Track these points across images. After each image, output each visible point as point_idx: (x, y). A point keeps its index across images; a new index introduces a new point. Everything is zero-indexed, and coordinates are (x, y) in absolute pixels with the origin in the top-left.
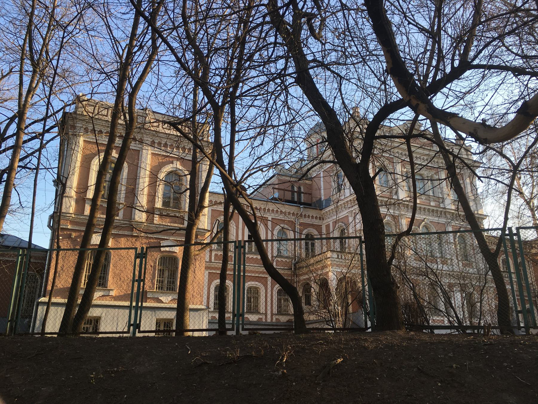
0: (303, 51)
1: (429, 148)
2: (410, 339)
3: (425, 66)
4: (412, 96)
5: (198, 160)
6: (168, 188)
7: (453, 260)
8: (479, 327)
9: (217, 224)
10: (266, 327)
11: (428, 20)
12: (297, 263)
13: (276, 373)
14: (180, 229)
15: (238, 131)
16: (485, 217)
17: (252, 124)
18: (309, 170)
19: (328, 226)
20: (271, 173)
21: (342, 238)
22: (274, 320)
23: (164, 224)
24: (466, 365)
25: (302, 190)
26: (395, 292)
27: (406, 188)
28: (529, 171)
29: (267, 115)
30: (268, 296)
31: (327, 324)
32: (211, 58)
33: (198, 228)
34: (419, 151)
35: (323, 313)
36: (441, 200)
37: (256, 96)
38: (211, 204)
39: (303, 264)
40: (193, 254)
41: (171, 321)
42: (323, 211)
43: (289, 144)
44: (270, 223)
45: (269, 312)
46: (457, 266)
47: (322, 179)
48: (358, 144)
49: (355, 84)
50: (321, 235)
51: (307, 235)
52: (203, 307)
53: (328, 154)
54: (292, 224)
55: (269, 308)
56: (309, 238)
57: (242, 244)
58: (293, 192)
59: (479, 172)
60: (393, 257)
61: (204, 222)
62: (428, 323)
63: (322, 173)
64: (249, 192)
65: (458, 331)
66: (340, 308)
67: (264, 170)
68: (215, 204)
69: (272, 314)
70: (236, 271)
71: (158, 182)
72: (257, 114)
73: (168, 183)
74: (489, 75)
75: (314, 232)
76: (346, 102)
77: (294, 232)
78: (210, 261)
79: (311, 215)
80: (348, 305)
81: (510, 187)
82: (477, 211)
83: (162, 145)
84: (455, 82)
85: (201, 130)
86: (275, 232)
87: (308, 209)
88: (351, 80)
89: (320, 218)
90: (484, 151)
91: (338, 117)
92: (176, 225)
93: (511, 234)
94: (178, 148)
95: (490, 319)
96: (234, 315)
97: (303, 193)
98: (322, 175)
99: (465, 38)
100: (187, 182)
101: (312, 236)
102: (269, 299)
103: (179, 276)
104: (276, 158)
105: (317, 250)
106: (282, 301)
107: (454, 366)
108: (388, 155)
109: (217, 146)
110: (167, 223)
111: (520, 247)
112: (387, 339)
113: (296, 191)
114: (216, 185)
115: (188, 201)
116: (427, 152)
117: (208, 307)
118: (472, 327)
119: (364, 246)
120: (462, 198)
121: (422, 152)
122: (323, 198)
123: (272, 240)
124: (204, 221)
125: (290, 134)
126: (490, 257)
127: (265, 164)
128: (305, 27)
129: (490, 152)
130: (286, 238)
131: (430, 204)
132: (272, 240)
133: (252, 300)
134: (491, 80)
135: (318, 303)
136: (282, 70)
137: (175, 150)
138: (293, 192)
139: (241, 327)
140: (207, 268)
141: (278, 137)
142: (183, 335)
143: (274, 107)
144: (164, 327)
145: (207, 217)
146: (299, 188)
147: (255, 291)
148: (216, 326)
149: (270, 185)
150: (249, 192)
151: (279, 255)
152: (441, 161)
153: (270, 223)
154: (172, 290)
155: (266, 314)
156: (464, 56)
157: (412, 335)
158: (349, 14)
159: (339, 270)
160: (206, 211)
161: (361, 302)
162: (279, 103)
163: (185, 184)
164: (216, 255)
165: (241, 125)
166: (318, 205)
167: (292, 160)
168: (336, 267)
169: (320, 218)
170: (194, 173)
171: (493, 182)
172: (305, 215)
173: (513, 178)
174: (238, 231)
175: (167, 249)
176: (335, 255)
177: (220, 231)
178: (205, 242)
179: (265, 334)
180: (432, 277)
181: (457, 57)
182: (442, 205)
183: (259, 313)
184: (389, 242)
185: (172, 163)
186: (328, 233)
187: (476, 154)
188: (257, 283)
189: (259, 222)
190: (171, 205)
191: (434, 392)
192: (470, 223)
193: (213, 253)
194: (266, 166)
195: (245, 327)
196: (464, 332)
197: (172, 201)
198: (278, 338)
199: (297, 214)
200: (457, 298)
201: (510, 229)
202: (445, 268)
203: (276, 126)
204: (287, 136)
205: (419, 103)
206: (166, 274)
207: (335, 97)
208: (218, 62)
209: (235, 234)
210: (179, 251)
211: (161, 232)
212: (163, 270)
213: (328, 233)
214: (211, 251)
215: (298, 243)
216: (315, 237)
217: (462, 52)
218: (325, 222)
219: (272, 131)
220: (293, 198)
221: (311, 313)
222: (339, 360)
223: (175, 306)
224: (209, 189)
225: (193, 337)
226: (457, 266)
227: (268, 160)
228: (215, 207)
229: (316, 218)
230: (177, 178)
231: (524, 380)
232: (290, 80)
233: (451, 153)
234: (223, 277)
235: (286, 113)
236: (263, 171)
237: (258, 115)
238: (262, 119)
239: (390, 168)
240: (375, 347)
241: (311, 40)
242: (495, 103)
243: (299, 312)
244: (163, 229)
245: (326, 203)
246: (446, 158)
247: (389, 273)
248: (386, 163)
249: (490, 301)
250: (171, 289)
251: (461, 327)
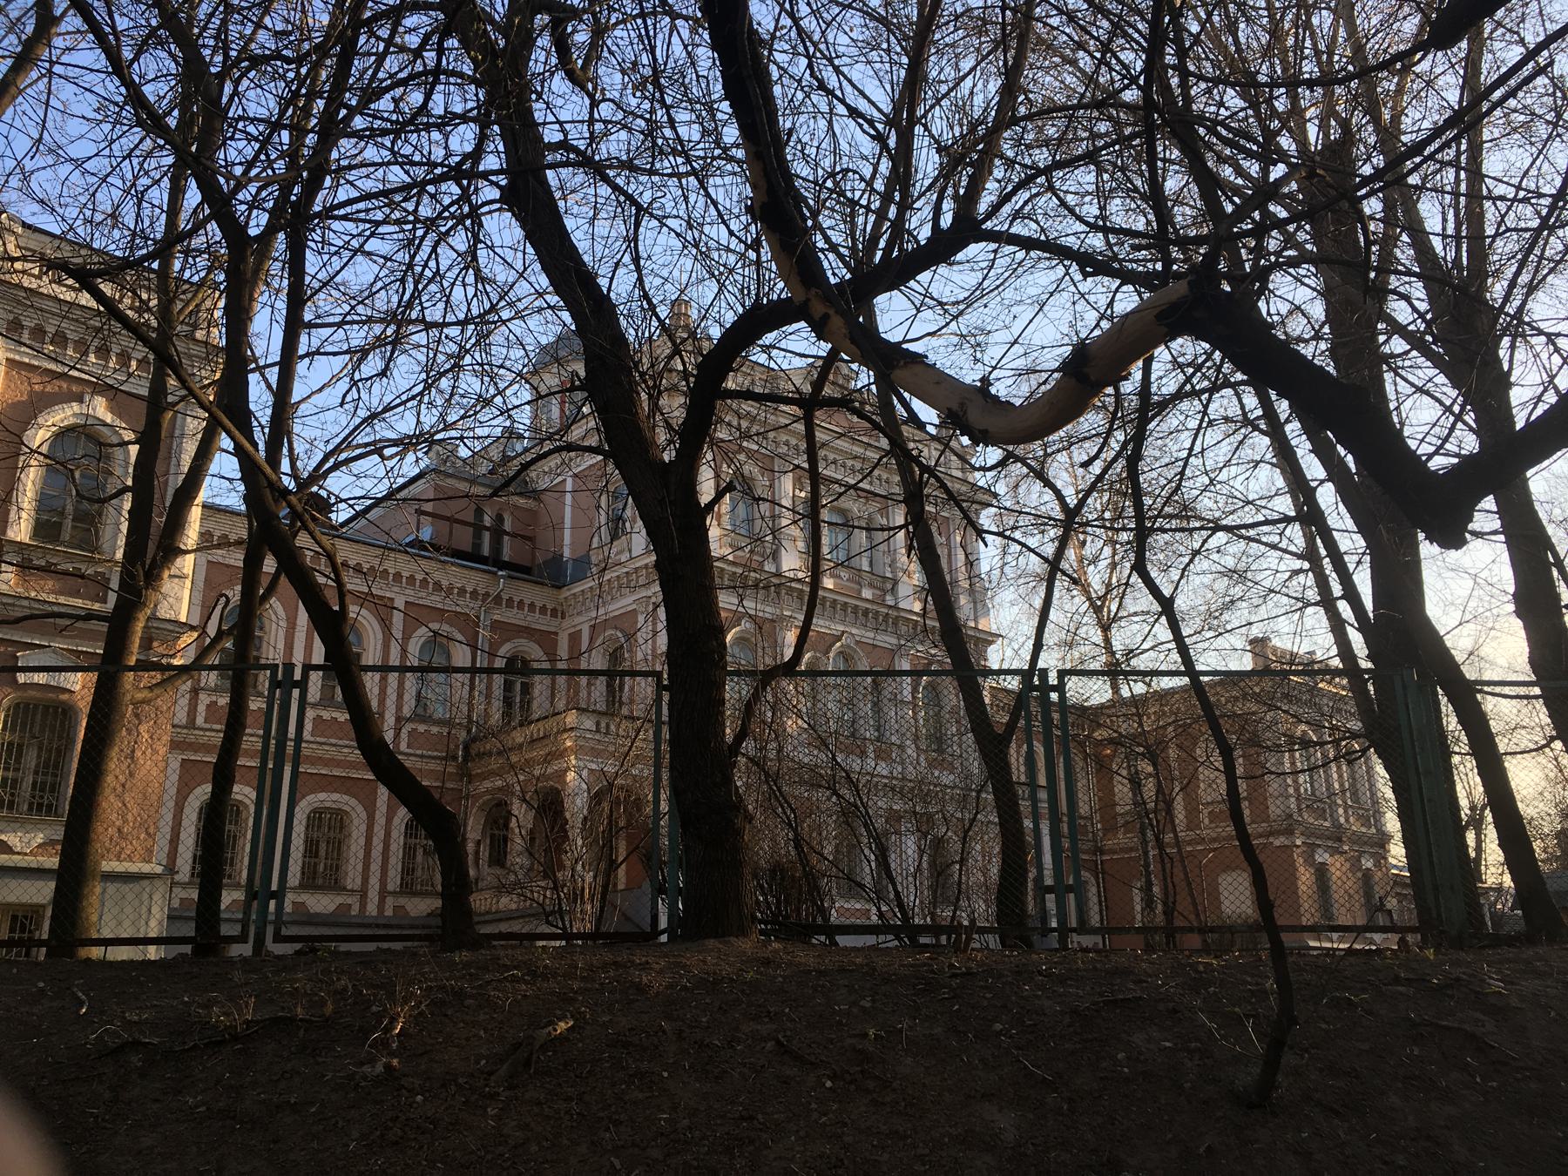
0: (530, 112)
1: (865, 439)
2: (767, 962)
3: (872, 218)
4: (813, 291)
5: (170, 399)
6: (61, 480)
7: (906, 748)
8: (953, 928)
9: (219, 608)
10: (355, 932)
11: (888, 87)
12: (474, 740)
13: (367, 1069)
14: (90, 616)
15: (310, 325)
16: (990, 638)
17: (360, 309)
18: (525, 467)
19: (575, 638)
20: (410, 466)
21: (615, 674)
22: (389, 912)
23: (33, 594)
24: (901, 1031)
25: (507, 526)
26: (739, 833)
27: (801, 545)
28: (1103, 527)
29: (410, 286)
30: (378, 833)
31: (548, 922)
32: (237, 83)
33: (153, 617)
34: (842, 444)
35: (541, 891)
36: (889, 586)
37: (378, 224)
38: (207, 542)
39: (491, 745)
40: (128, 697)
41: (35, 911)
42: (565, 593)
43: (471, 383)
44: (398, 618)
45: (374, 881)
46: (913, 761)
47: (568, 497)
48: (675, 407)
49: (678, 235)
50: (553, 661)
51: (511, 661)
52: (159, 869)
53: (586, 429)
54: (468, 625)
55: (375, 867)
56: (517, 667)
57: (297, 676)
58: (478, 528)
59: (986, 519)
60: (741, 736)
61: (179, 600)
62: (826, 919)
63: (569, 481)
64: (341, 514)
65: (898, 938)
66: (589, 877)
67: (388, 452)
68: (219, 546)
69: (383, 893)
70: (271, 756)
71: (22, 458)
72: (377, 279)
73: (56, 463)
74: (1028, 264)
75: (534, 652)
76: (651, 282)
77: (474, 648)
78: (191, 724)
79: (527, 602)
80: (613, 865)
81: (1054, 565)
82: (976, 620)
83: (47, 340)
84: (943, 269)
85: (187, 303)
86: (414, 647)
87: (520, 583)
88: (670, 222)
89: (554, 611)
90: (1002, 464)
91: (623, 323)
92: (79, 602)
93: (1045, 688)
94: (103, 352)
95: (982, 909)
96: (252, 895)
97: (508, 534)
98: (569, 487)
99: (971, 155)
100: (127, 467)
101: (525, 662)
102: (378, 843)
103: (75, 765)
104: (429, 419)
105: (539, 705)
106: (420, 852)
107: (871, 1032)
108: (755, 447)
109: (237, 359)
110: (45, 592)
111: (1064, 724)
112: (704, 962)
113: (481, 520)
114: (223, 485)
115: (124, 527)
116: (858, 450)
117: (171, 869)
118: (935, 929)
119: (666, 697)
120: (938, 589)
121: (847, 448)
122: (567, 553)
123: (403, 669)
124: (178, 595)
125: (477, 355)
126: (992, 745)
127: (393, 436)
128: (544, 41)
129: (1017, 469)
130: (445, 663)
131: (860, 592)
132: (403, 669)
133: (323, 846)
134: (1030, 278)
135: (527, 863)
136: (466, 157)
137: (92, 358)
138: (478, 528)
139: (270, 930)
140: (175, 745)
141: (441, 358)
142: (72, 955)
143: (432, 264)
144: (12, 930)
145: (188, 583)
146: (499, 519)
147: (328, 826)
148: (189, 930)
149: (404, 500)
150: (341, 514)
151: (421, 715)
152: (889, 481)
153: (398, 618)
154: (48, 813)
155: (363, 893)
156: (966, 203)
157: (776, 951)
158: (673, 28)
159: (594, 766)
160: (187, 563)
161: (647, 857)
162: (446, 256)
163: (118, 471)
164: (211, 706)
165: (323, 304)
166: (552, 573)
167: (479, 432)
168: (589, 756)
169: (554, 613)
170: (152, 440)
171: (1016, 548)
172: (510, 600)
173: (1063, 543)
174: (287, 634)
175: (40, 678)
176: (589, 723)
177: (229, 632)
178: (176, 662)
179: (348, 953)
180: (844, 792)
181: (948, 205)
182: (890, 600)
183: (345, 889)
184: (734, 691)
185: (81, 400)
186: (575, 655)
187: (984, 469)
188: (336, 796)
189: (353, 610)
190: (66, 535)
191: (814, 1106)
192: (950, 651)
193: (204, 699)
194: (395, 443)
195: (284, 932)
196: (913, 940)
197: (68, 523)
198: (384, 962)
199: (487, 595)
200: (908, 850)
201: (1044, 672)
202: (883, 769)
203: (435, 325)
204: (468, 359)
205: (831, 312)
206: (31, 759)
207: (617, 265)
208: (258, 100)
209: (281, 646)
210: (79, 685)
211: (18, 621)
212: (20, 746)
213: (575, 655)
214: (195, 691)
215: (481, 682)
216: (535, 665)
217: (962, 191)
218: (566, 623)
219: (421, 338)
220: (477, 545)
221: (501, 889)
222: (562, 1026)
223: (53, 862)
224: (203, 496)
225: (104, 964)
226: (913, 761)
227: (404, 424)
228: (219, 555)
229: (543, 610)
230: (92, 448)
231: (1038, 1068)
232: (489, 193)
233: (916, 460)
234: (223, 775)
235: (471, 291)
236: (383, 458)
237: (379, 284)
238: (395, 299)
239: (761, 484)
240: (671, 986)
241: (559, 83)
242: (1038, 340)
243: (457, 887)
244: (27, 612)
245: (573, 569)
246: (904, 471)
247: (729, 780)
248: (750, 469)
249: (984, 862)
250: (42, 808)
251: (907, 930)
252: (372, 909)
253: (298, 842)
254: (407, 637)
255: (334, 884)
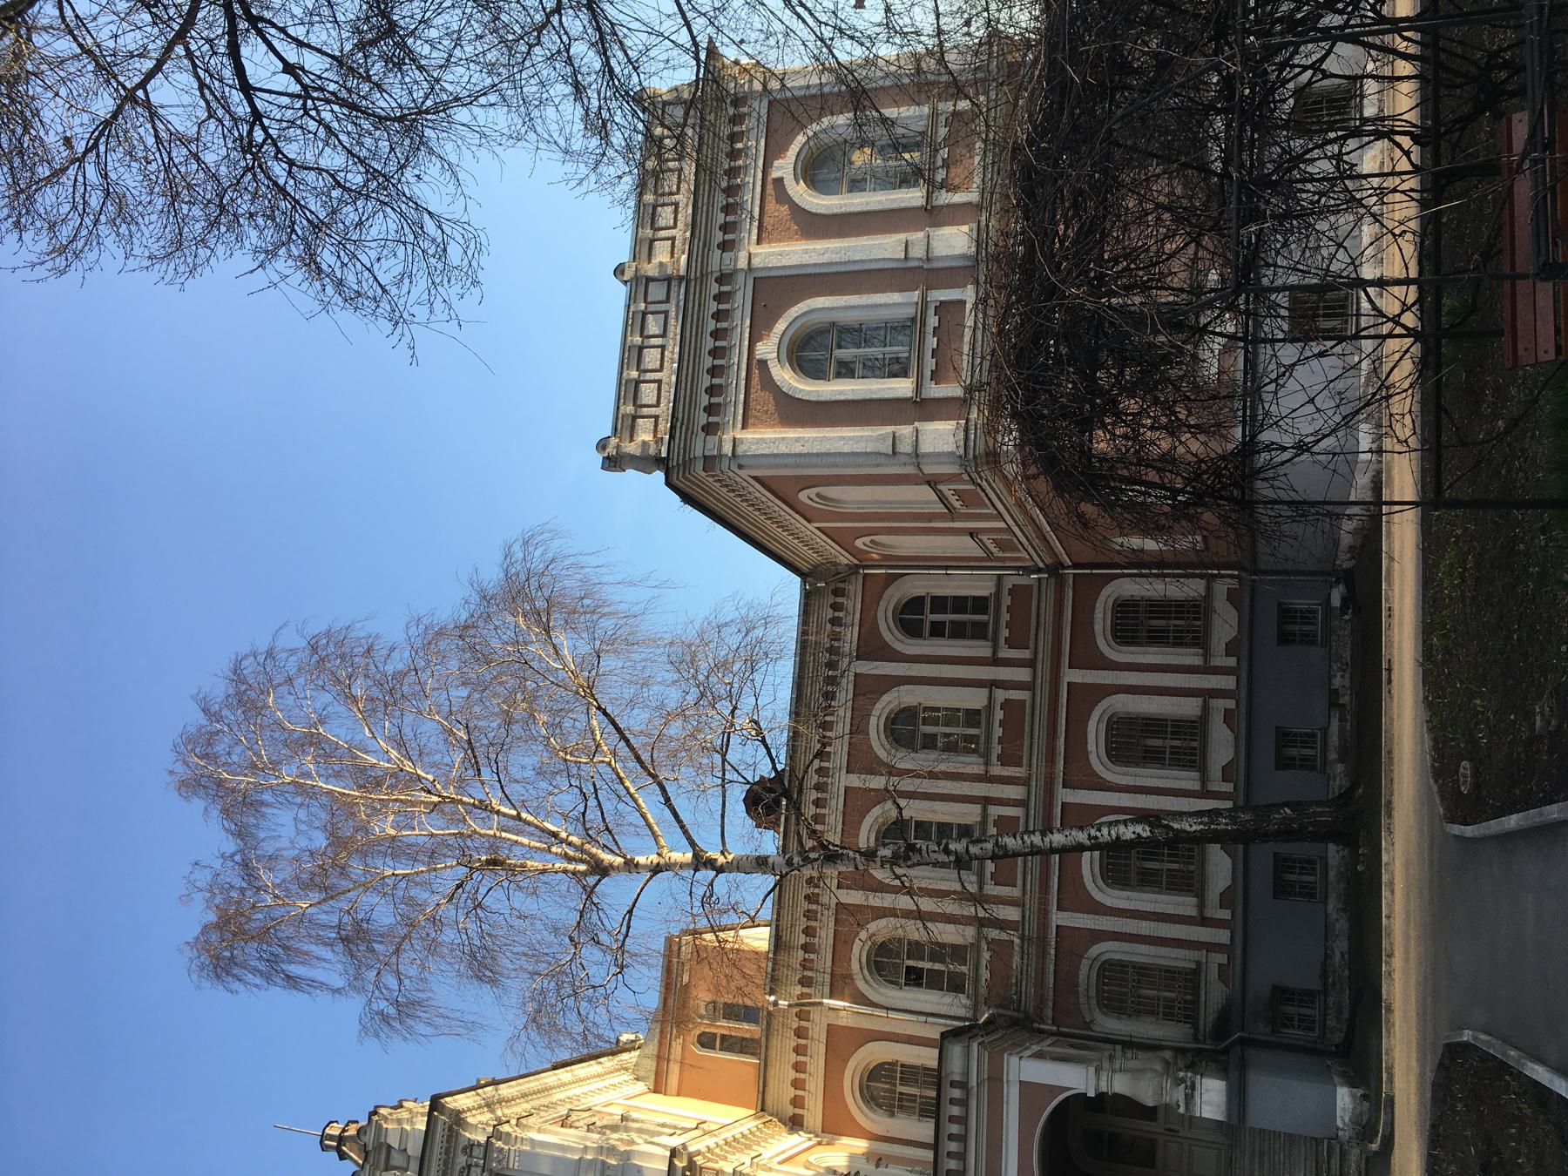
102: (1145, 928)
164: (997, 879)
252: (1228, 682)
253: (1152, 655)
254: (892, 771)
255: (1194, 729)
